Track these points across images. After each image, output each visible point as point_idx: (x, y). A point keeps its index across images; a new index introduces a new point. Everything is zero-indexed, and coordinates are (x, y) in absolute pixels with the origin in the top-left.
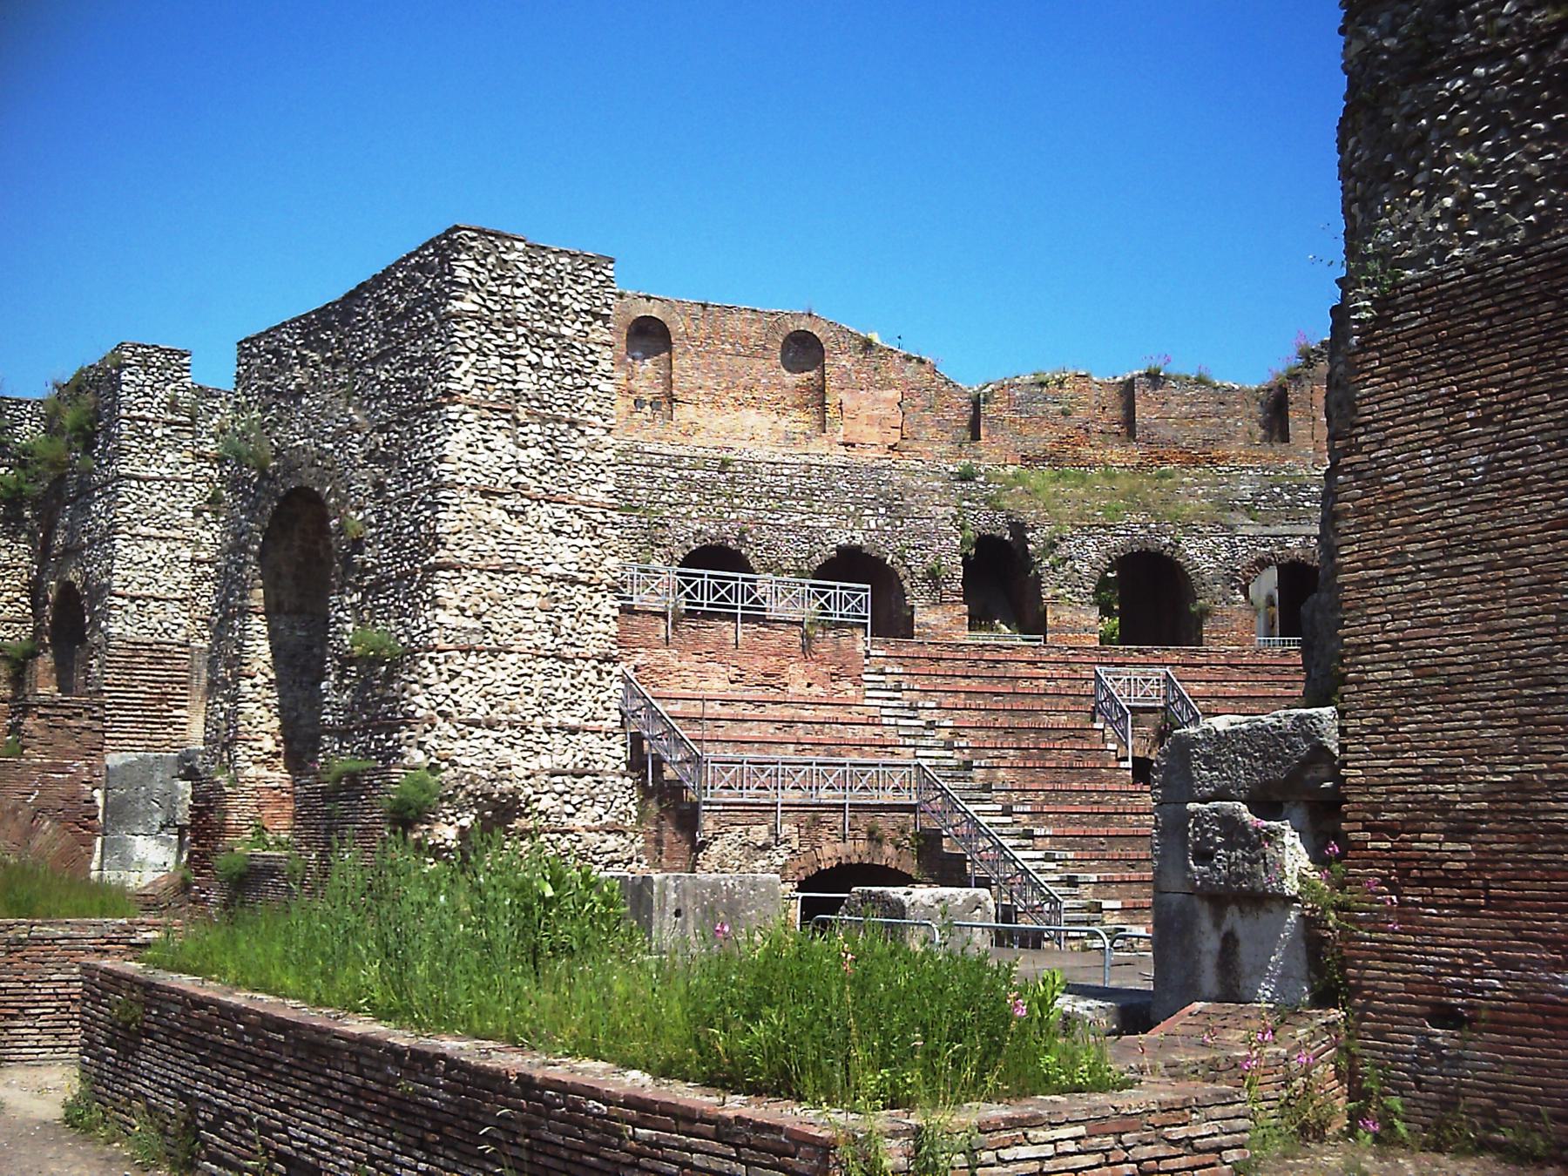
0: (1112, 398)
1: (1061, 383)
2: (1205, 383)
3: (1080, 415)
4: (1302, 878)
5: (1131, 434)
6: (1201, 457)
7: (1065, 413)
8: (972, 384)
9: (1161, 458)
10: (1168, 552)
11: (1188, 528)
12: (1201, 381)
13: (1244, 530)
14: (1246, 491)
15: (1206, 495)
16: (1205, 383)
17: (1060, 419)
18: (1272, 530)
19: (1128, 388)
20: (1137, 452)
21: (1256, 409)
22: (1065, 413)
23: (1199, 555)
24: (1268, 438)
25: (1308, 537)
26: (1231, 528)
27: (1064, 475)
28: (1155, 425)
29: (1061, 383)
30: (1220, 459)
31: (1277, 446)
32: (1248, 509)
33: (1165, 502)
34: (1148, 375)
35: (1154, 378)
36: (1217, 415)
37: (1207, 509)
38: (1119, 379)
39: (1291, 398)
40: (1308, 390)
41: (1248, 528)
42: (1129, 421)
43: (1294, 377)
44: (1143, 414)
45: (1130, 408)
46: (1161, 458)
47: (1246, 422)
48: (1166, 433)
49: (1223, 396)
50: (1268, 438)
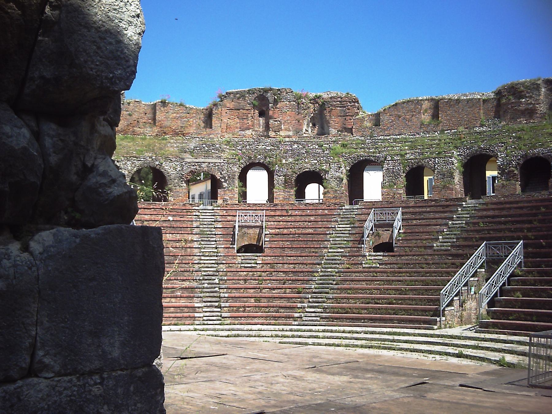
0: (149, 111)
1: (129, 104)
2: (183, 106)
3: (135, 116)
4: (111, 192)
5: (155, 123)
6: (179, 133)
7: (130, 115)
8: (204, 105)
9: (165, 133)
10: (158, 167)
11: (167, 159)
12: (181, 105)
13: (189, 160)
14: (192, 145)
15: (178, 147)
16: (183, 106)
17: (128, 117)
18: (197, 161)
19: (155, 105)
20: (156, 130)
21: (202, 116)
22: (130, 115)
23: (170, 169)
24: (205, 127)
25: (209, 163)
26: (183, 159)
27: (126, 138)
28: (163, 120)
29: (129, 104)
30: (186, 134)
31: (208, 130)
32: (191, 152)
33: (161, 149)
34: (161, 102)
35: (164, 103)
36: (186, 117)
37: (176, 152)
38: (152, 103)
39: (214, 112)
40: (220, 110)
41: (189, 158)
42: (154, 119)
43: (215, 105)
44: (160, 116)
45: (154, 114)
46: (165, 133)
47: (198, 121)
48: (167, 123)
49: (189, 111)
50: (205, 127)
